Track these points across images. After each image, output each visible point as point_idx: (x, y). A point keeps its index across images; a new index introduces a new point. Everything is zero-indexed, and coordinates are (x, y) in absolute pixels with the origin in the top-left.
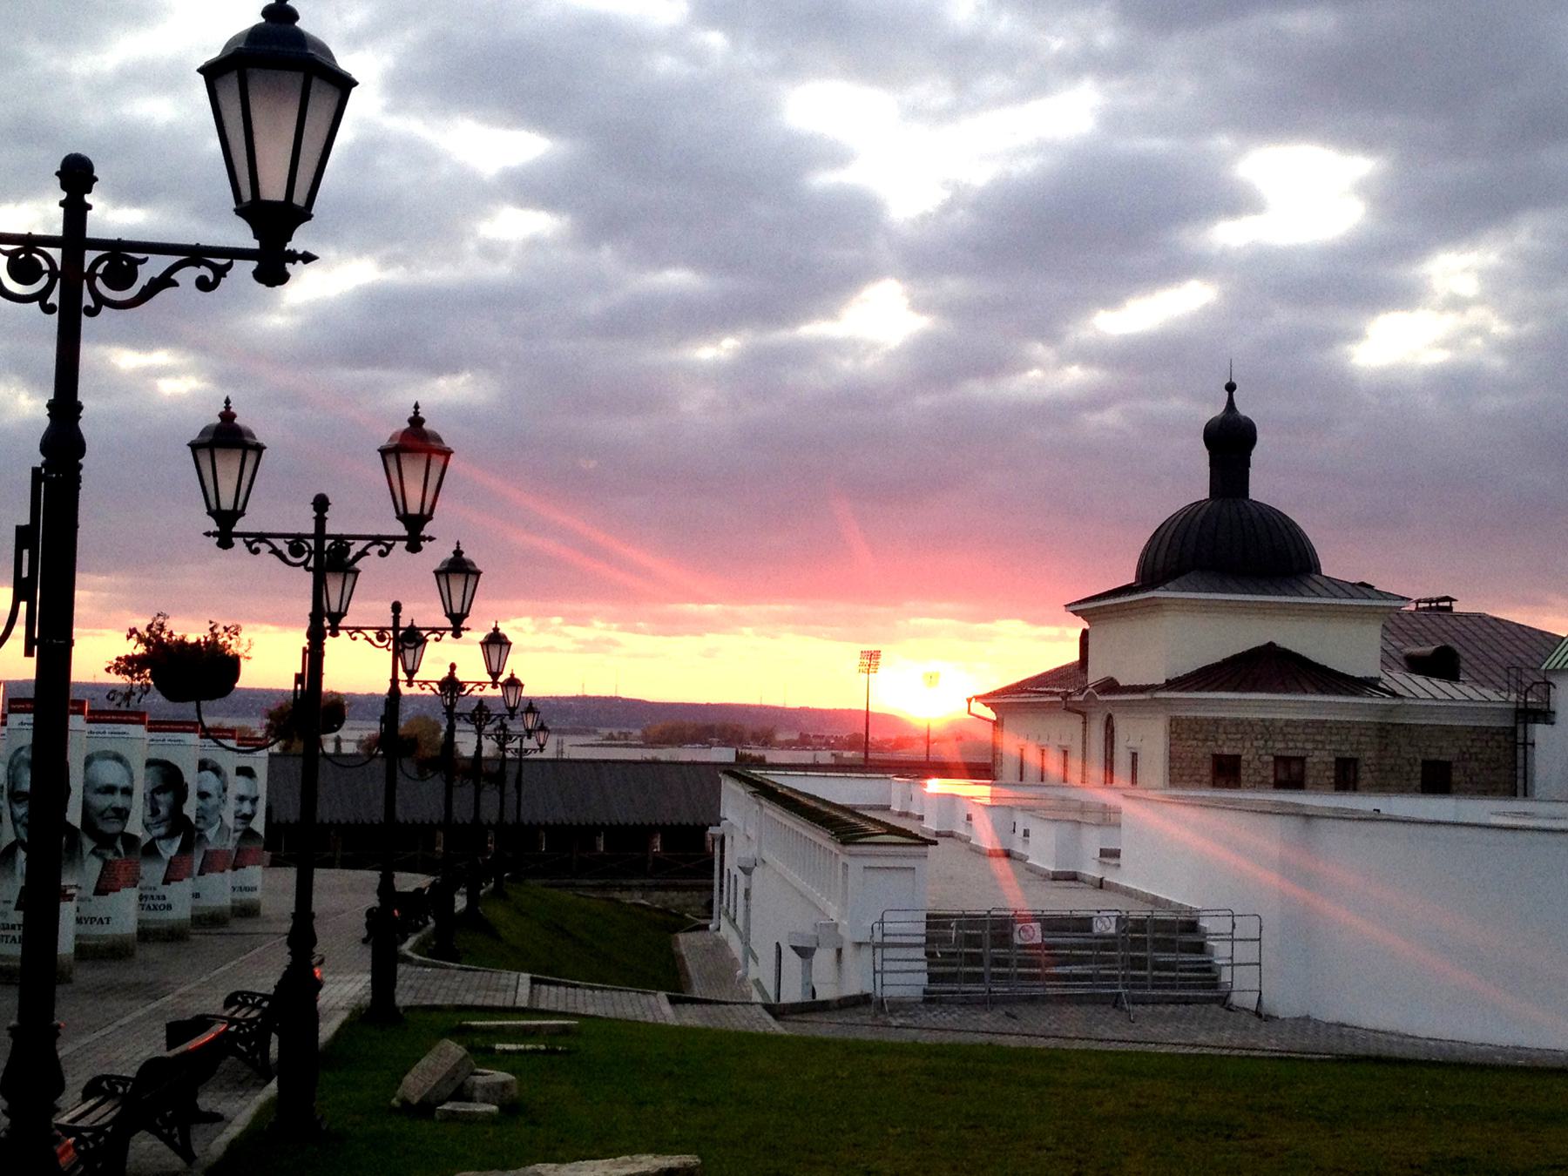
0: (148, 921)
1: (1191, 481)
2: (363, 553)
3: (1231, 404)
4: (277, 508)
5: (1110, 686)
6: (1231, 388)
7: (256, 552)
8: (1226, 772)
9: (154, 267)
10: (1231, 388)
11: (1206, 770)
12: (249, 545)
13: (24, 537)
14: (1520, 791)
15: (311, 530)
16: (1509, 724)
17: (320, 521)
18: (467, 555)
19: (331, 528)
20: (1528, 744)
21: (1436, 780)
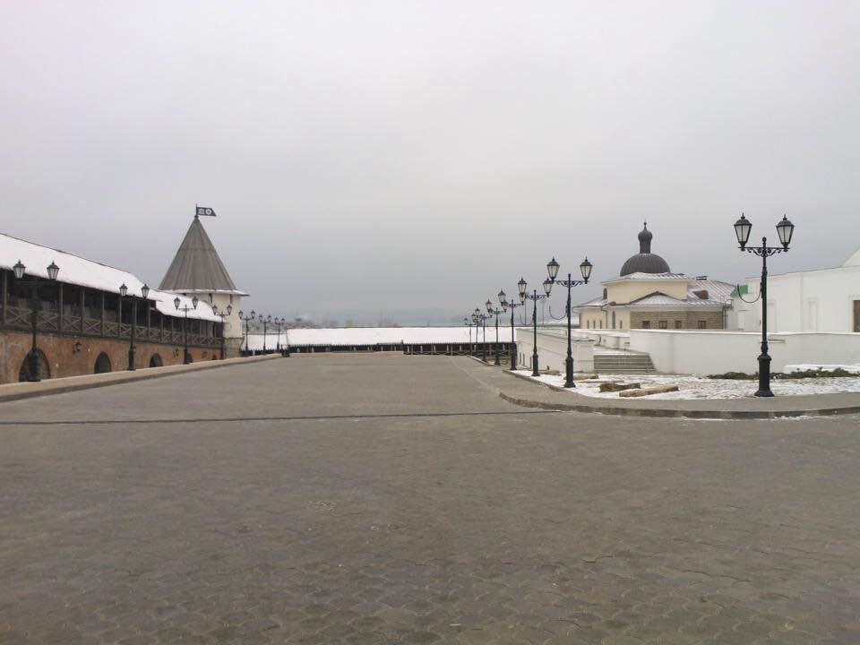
1: (634, 249)
3: (645, 228)
4: (754, 241)
5: (613, 304)
6: (645, 224)
8: (646, 325)
10: (645, 224)
11: (641, 324)
14: (42, 370)
17: (764, 244)
18: (556, 260)
19: (767, 246)
21: (702, 325)
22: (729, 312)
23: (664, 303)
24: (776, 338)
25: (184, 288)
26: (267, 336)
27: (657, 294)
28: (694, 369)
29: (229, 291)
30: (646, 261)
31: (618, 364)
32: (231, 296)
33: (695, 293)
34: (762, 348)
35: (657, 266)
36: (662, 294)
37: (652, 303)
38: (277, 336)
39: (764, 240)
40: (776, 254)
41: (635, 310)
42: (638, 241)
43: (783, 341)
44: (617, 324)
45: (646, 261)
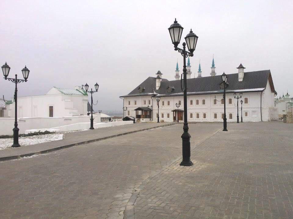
9: (20, 81)
17: (16, 77)
22: (5, 111)
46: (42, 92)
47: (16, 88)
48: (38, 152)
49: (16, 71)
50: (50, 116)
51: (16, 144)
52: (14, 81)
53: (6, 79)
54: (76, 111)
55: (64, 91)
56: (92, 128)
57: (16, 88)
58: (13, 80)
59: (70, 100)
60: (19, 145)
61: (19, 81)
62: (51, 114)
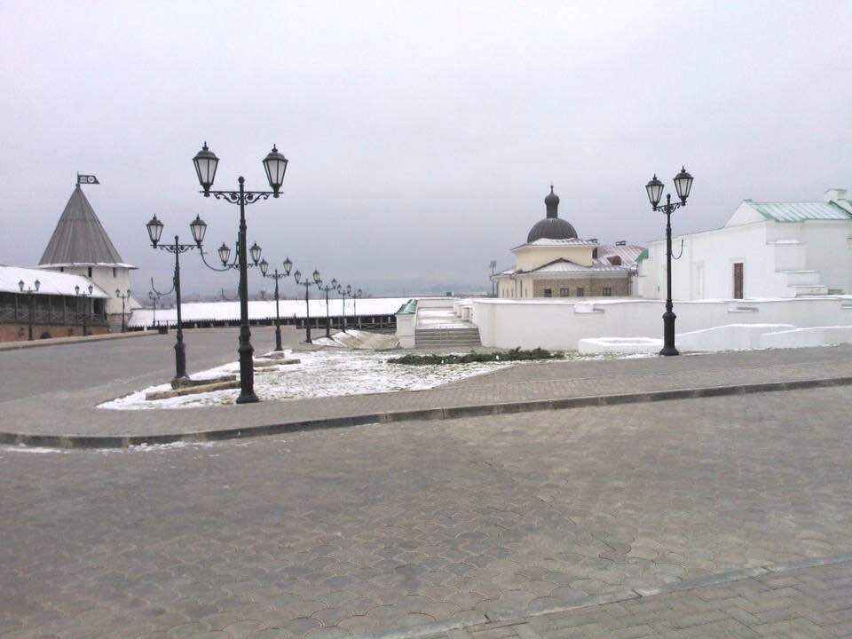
0: (390, 333)
1: (541, 214)
2: (258, 198)
4: (167, 238)
6: (552, 187)
7: (219, 198)
8: (548, 293)
9: (255, 196)
10: (552, 187)
11: (543, 293)
12: (216, 196)
13: (237, 244)
15: (238, 190)
16: (626, 277)
17: (242, 187)
19: (180, 243)
20: (631, 282)
22: (634, 278)
23: (566, 270)
24: (747, 306)
25: (62, 262)
26: (156, 311)
27: (561, 260)
28: (615, 334)
29: (112, 265)
30: (553, 227)
31: (445, 339)
32: (114, 269)
33: (609, 259)
34: (177, 337)
35: (564, 231)
36: (567, 261)
37: (557, 270)
38: (152, 312)
39: (177, 238)
40: (190, 250)
41: (537, 279)
42: (545, 206)
43: (603, 311)
44: (524, 294)
45: (553, 227)
46: (718, 225)
47: (243, 221)
48: (195, 434)
49: (241, 164)
50: (736, 297)
51: (248, 395)
52: (234, 198)
53: (207, 194)
54: (811, 278)
55: (776, 212)
56: (670, 349)
57: (243, 221)
58: (230, 197)
59: (795, 242)
60: (255, 397)
61: (250, 198)
62: (739, 283)
